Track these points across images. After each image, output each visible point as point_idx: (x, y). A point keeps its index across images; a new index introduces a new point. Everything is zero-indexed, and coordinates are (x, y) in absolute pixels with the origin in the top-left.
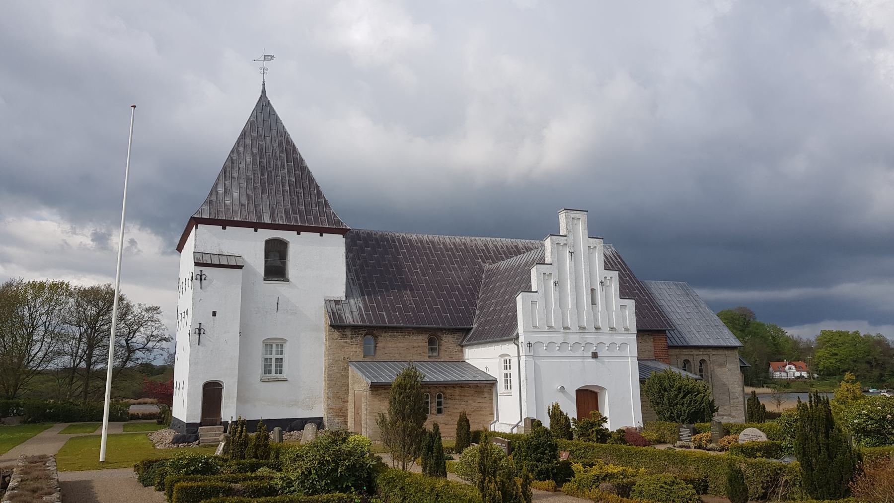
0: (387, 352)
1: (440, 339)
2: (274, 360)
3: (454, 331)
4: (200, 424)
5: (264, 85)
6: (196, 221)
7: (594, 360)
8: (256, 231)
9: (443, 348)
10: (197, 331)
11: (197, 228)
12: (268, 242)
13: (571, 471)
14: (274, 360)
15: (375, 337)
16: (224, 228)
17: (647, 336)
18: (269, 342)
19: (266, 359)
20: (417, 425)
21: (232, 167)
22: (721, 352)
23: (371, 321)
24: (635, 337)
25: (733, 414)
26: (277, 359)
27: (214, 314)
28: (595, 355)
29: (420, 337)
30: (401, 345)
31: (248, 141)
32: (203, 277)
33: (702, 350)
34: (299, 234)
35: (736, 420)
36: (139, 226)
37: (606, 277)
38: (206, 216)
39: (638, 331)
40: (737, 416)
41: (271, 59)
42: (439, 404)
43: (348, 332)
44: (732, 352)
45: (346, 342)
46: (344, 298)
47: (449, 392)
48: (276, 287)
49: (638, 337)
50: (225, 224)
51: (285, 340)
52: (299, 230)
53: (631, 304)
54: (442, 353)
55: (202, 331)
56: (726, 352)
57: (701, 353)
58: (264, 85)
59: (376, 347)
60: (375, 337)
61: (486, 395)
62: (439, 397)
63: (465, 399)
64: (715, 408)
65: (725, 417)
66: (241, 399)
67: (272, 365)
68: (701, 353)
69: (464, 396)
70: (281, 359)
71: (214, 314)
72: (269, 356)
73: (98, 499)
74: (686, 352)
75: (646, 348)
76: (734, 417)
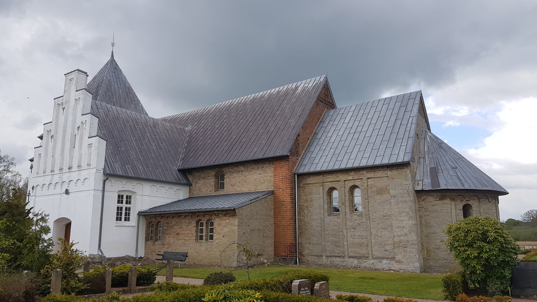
13: (466, 293)
17: (268, 165)
18: (121, 194)
20: (480, 241)
22: (380, 173)
25: (398, 257)
28: (67, 192)
33: (353, 173)
35: (403, 266)
40: (405, 261)
44: (400, 171)
56: (389, 173)
57: (350, 178)
65: (385, 261)
67: (119, 204)
68: (350, 178)
73: (74, 248)
74: (330, 178)
75: (266, 178)
76: (399, 262)
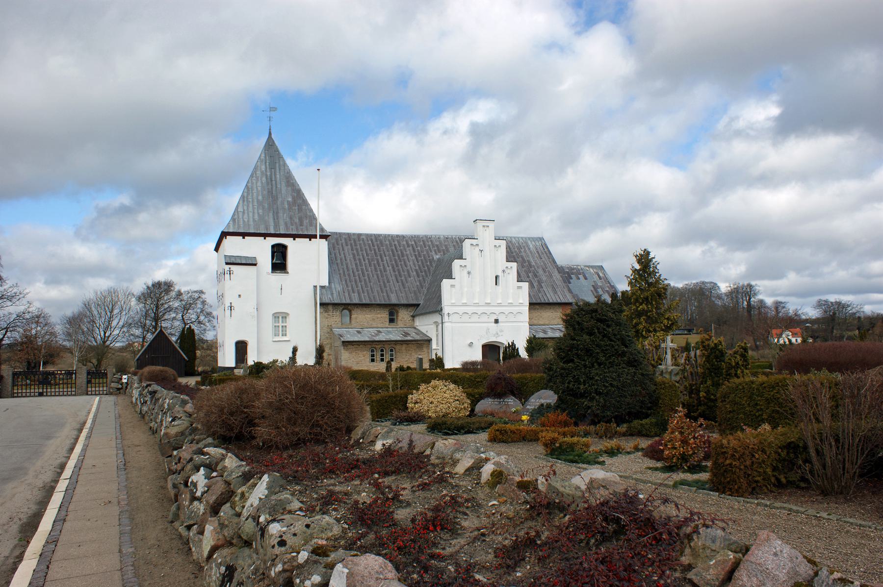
0: (358, 321)
1: (397, 312)
2: (280, 327)
3: (407, 306)
4: (235, 368)
5: (270, 129)
6: (224, 235)
7: (496, 325)
8: (265, 239)
9: (400, 318)
10: (230, 308)
11: (226, 238)
12: (273, 246)
14: (280, 327)
15: (350, 311)
16: (244, 238)
19: (275, 326)
21: (248, 194)
23: (371, 301)
24: (527, 308)
26: (282, 326)
27: (240, 296)
28: (497, 321)
29: (383, 311)
30: (369, 316)
31: (259, 173)
32: (231, 272)
34: (310, 240)
36: (790, 315)
37: (507, 267)
38: (231, 230)
39: (531, 304)
41: (274, 111)
42: (382, 355)
43: (330, 308)
45: (329, 315)
46: (327, 284)
47: (398, 347)
48: (279, 277)
49: (530, 309)
50: (244, 235)
51: (288, 314)
52: (294, 237)
53: (525, 286)
54: (399, 322)
55: (232, 308)
58: (270, 129)
59: (350, 318)
60: (350, 311)
61: (425, 349)
62: (382, 351)
63: (410, 352)
64: (787, 343)
66: (259, 352)
69: (409, 350)
70: (286, 326)
71: (240, 296)
72: (277, 324)
